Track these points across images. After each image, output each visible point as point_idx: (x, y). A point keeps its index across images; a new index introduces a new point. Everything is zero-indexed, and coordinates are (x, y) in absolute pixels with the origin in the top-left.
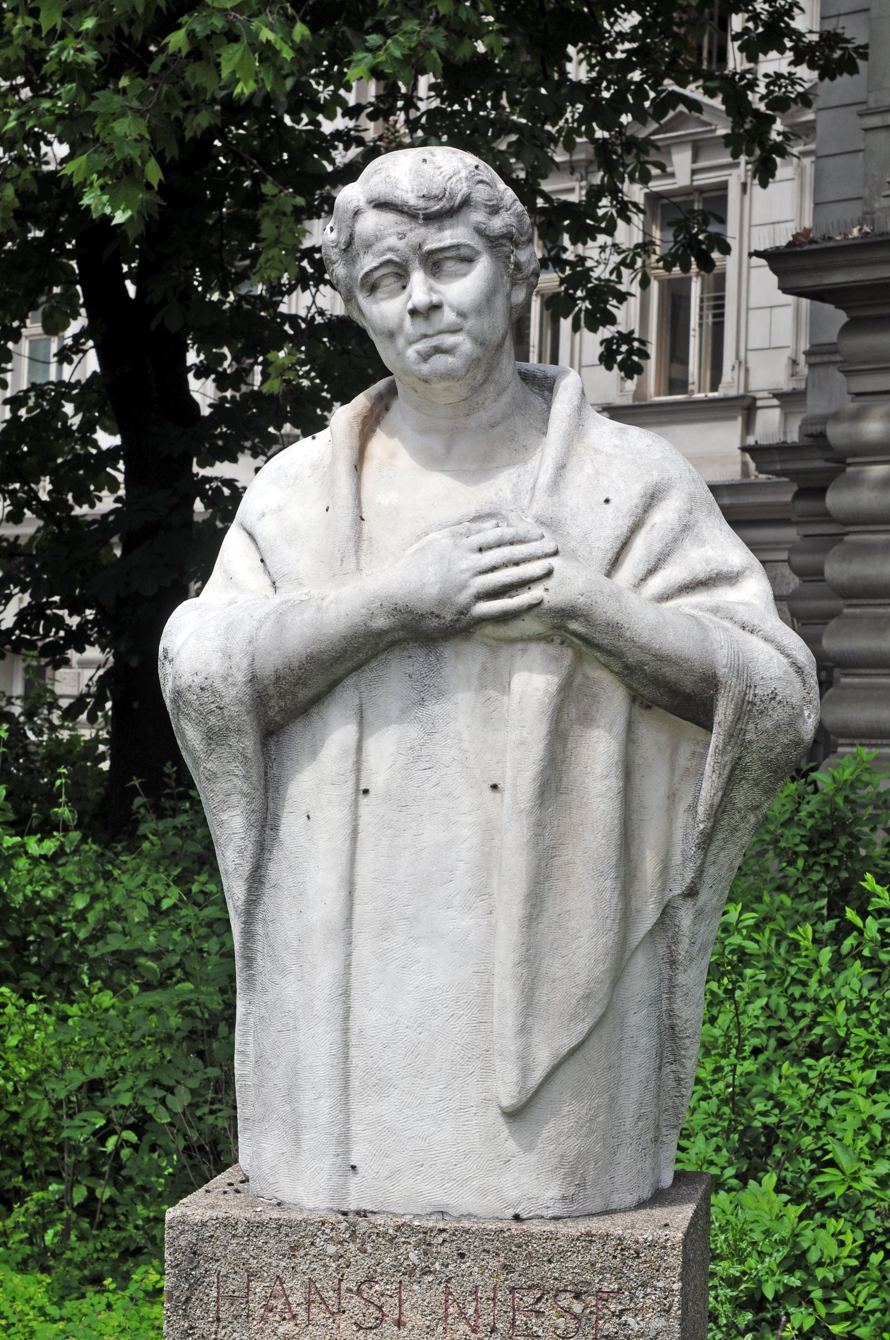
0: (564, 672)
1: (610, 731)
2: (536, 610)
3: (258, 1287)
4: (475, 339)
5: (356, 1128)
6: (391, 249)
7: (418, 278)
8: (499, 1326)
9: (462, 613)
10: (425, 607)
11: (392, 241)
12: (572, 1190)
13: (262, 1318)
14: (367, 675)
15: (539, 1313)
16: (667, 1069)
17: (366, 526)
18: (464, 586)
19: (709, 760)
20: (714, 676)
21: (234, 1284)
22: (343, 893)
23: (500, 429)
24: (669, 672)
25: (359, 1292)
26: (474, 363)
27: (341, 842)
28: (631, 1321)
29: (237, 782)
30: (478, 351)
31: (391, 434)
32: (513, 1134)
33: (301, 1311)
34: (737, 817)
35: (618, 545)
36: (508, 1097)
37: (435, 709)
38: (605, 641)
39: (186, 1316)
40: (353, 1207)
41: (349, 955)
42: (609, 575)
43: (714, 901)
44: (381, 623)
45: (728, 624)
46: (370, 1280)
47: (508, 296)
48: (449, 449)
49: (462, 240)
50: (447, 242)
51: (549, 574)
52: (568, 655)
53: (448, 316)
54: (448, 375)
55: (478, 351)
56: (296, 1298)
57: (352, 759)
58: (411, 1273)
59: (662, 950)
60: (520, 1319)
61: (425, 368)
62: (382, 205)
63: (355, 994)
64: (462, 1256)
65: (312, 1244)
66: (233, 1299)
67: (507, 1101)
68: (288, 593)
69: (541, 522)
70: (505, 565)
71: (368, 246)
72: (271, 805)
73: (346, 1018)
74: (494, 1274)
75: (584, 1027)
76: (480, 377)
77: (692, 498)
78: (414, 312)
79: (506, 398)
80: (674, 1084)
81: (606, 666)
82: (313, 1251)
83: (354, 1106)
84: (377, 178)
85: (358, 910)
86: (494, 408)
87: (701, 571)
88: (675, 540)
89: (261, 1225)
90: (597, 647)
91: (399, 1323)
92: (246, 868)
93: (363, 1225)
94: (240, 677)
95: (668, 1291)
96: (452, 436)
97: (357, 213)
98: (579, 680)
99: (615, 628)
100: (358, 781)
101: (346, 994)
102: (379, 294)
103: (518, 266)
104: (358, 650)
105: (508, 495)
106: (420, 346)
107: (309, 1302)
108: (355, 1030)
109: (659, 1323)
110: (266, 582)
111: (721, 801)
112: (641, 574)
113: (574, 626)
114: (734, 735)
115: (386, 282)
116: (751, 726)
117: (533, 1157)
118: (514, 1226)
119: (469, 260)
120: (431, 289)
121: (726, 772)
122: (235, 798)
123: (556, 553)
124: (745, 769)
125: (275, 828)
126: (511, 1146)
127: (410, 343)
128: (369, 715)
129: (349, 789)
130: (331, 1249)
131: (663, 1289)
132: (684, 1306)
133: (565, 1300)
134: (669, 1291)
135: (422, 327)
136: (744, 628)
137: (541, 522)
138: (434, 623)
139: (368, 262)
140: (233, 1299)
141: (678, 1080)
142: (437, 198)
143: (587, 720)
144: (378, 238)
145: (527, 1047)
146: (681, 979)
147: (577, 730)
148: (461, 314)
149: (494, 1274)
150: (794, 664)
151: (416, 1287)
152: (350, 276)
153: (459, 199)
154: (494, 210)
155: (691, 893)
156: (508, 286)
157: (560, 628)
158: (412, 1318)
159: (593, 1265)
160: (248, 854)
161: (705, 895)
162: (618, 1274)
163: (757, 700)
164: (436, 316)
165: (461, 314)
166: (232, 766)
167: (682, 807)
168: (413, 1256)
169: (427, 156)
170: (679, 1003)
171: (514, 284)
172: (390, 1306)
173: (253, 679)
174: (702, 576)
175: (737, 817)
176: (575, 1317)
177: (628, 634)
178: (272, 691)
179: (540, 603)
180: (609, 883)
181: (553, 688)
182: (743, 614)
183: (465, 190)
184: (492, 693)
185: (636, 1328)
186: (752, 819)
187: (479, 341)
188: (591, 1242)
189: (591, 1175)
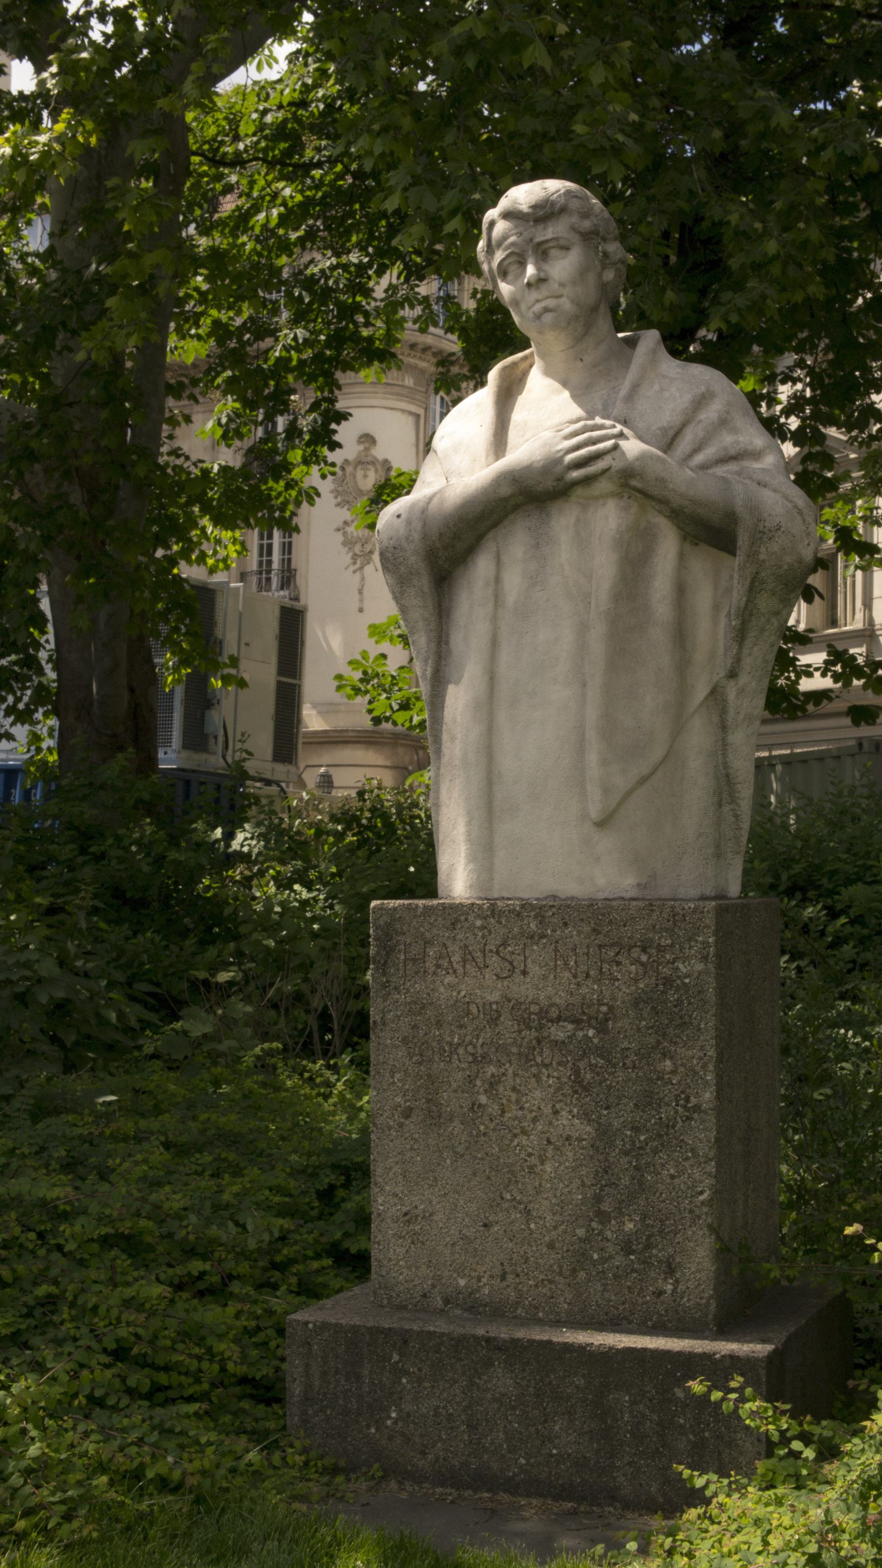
2: (608, 474)
4: (572, 302)
8: (592, 973)
9: (559, 480)
13: (434, 973)
15: (618, 963)
16: (726, 809)
21: (415, 951)
25: (498, 953)
28: (681, 966)
34: (763, 619)
36: (595, 812)
38: (655, 491)
40: (496, 895)
43: (754, 684)
45: (748, 482)
46: (504, 944)
47: (600, 275)
49: (560, 235)
56: (456, 958)
60: (606, 967)
65: (466, 920)
66: (414, 960)
72: (444, 627)
80: (734, 819)
81: (660, 512)
82: (466, 925)
91: (524, 973)
94: (416, 536)
107: (465, 961)
109: (700, 967)
111: (746, 605)
113: (634, 483)
114: (752, 555)
121: (747, 583)
125: (447, 643)
130: (479, 923)
132: (718, 955)
133: (636, 953)
134: (706, 944)
136: (759, 484)
141: (736, 816)
148: (562, 285)
151: (535, 947)
155: (732, 674)
157: (625, 485)
159: (654, 927)
163: (766, 530)
168: (533, 926)
171: (604, 267)
172: (518, 960)
173: (425, 537)
174: (732, 452)
175: (763, 619)
176: (643, 964)
177: (671, 486)
179: (608, 469)
185: (684, 970)
188: (652, 910)
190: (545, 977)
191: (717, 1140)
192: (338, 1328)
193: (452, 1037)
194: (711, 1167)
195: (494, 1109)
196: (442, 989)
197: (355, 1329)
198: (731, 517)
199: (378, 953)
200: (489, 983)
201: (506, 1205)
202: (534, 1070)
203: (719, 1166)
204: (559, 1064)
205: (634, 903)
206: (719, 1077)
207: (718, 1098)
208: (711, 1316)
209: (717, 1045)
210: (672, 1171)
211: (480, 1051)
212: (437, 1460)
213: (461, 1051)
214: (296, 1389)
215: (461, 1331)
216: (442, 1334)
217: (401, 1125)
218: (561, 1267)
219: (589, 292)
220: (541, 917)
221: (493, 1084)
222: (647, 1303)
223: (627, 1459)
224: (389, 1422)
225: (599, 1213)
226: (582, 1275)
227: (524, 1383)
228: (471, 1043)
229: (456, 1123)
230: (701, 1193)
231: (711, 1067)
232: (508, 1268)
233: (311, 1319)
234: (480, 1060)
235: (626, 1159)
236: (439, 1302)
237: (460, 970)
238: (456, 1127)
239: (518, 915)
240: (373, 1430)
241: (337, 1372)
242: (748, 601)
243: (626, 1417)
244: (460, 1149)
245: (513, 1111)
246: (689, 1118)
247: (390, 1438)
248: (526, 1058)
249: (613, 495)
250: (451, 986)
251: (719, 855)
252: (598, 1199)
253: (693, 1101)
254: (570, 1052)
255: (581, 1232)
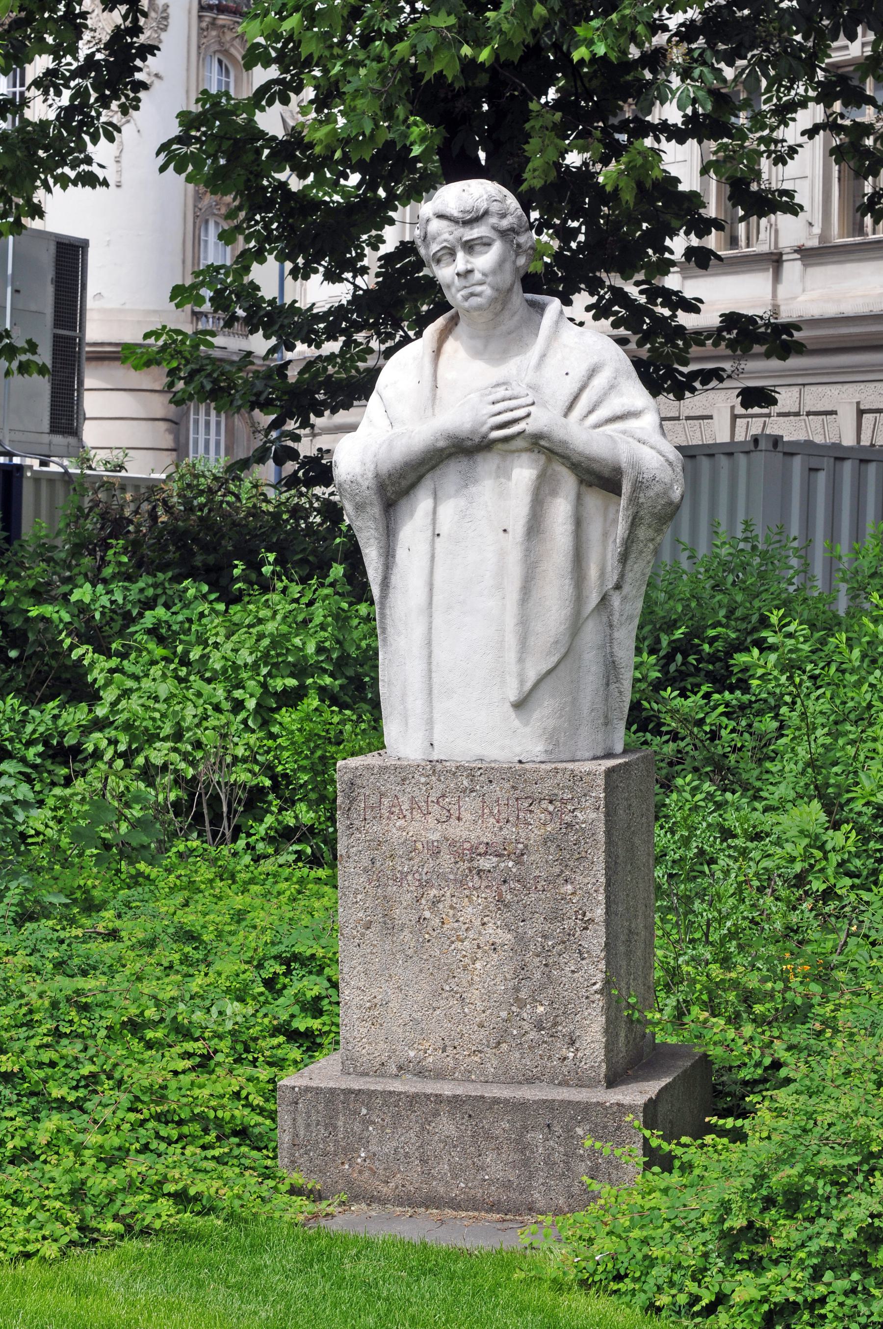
0: (540, 468)
1: (566, 499)
3: (386, 801)
4: (493, 288)
5: (436, 715)
6: (445, 241)
7: (460, 255)
10: (464, 435)
11: (446, 236)
12: (551, 747)
13: (388, 818)
14: (438, 472)
16: (613, 687)
17: (438, 391)
18: (484, 423)
19: (621, 514)
20: (620, 468)
22: (427, 589)
23: (514, 335)
24: (595, 466)
25: (438, 803)
26: (493, 301)
27: (425, 562)
28: (579, 815)
29: (372, 532)
30: (496, 294)
31: (456, 339)
32: (517, 716)
33: (407, 813)
34: (641, 545)
35: (572, 398)
36: (513, 695)
37: (473, 489)
39: (348, 818)
40: (436, 758)
41: (431, 623)
42: (566, 415)
44: (441, 444)
45: (630, 440)
46: (443, 796)
47: (514, 262)
48: (486, 346)
49: (483, 234)
50: (475, 236)
51: (528, 415)
52: (543, 459)
53: (477, 276)
54: (479, 308)
55: (496, 294)
56: (405, 807)
57: (431, 517)
58: (464, 791)
59: (605, 619)
60: (522, 814)
61: (466, 304)
62: (441, 216)
63: (434, 644)
64: (491, 782)
66: (372, 808)
67: (513, 698)
68: (398, 429)
69: (530, 387)
70: (506, 411)
71: (434, 239)
73: (430, 657)
74: (507, 791)
75: (555, 659)
76: (499, 307)
77: (617, 370)
78: (458, 274)
79: (516, 318)
82: (413, 781)
83: (435, 704)
84: (438, 201)
85: (435, 598)
86: (509, 323)
87: (618, 411)
88: (605, 394)
89: (386, 768)
90: (556, 454)
91: (459, 819)
92: (379, 579)
93: (439, 767)
94: (370, 475)
95: (598, 799)
96: (487, 339)
97: (428, 221)
98: (549, 472)
99: (564, 443)
100: (434, 529)
101: (429, 643)
102: (442, 264)
103: (519, 246)
104: (431, 459)
105: (514, 372)
106: (463, 293)
107: (412, 809)
108: (434, 663)
109: (593, 815)
110: (388, 422)
112: (584, 413)
113: (542, 443)
114: (633, 500)
115: (444, 258)
116: (642, 495)
117: (528, 729)
118: (518, 766)
119: (489, 245)
120: (467, 262)
122: (372, 541)
123: (533, 404)
124: (641, 519)
125: (394, 556)
126: (517, 723)
127: (459, 291)
128: (439, 494)
129: (429, 533)
130: (423, 780)
131: (595, 797)
132: (606, 806)
133: (544, 805)
135: (463, 282)
137: (530, 387)
138: (469, 443)
139: (435, 248)
140: (372, 808)
141: (620, 692)
142: (469, 212)
143: (554, 493)
144: (439, 235)
145: (523, 669)
146: (616, 635)
147: (549, 499)
148: (484, 274)
149: (507, 791)
150: (667, 460)
152: (427, 254)
153: (481, 211)
154: (503, 216)
155: (618, 587)
156: (514, 257)
157: (536, 444)
158: (466, 816)
160: (380, 571)
161: (626, 588)
162: (572, 790)
164: (470, 276)
165: (484, 274)
166: (369, 524)
167: (611, 540)
169: (466, 188)
170: (616, 649)
173: (377, 476)
174: (619, 413)
178: (387, 482)
179: (524, 431)
180: (567, 581)
181: (534, 477)
182: (639, 434)
183: (485, 206)
184: (503, 480)
186: (651, 546)
187: (497, 289)
189: (562, 740)
190: (475, 822)
191: (606, 944)
192: (318, 1091)
193: (403, 867)
194: (602, 966)
195: (436, 922)
196: (394, 830)
197: (332, 1091)
198: (618, 471)
199: (343, 803)
200: (432, 826)
201: (445, 995)
202: (467, 892)
203: (608, 965)
204: (486, 887)
205: (543, 766)
206: (608, 898)
207: (607, 913)
208: (602, 1076)
209: (606, 874)
210: (573, 968)
211: (425, 877)
212: (397, 1187)
213: (410, 877)
214: (285, 1138)
215: (413, 1090)
216: (400, 1093)
217: (363, 935)
218: (488, 1041)
219: (507, 277)
220: (471, 777)
221: (435, 902)
222: (554, 1067)
223: (541, 1181)
224: (359, 1160)
225: (517, 999)
226: (504, 1046)
227: (463, 1127)
228: (417, 871)
229: (406, 932)
230: (595, 984)
231: (602, 890)
232: (448, 1043)
233: (297, 1084)
234: (424, 885)
235: (538, 959)
236: (394, 1070)
237: (409, 816)
238: (406, 935)
239: (454, 774)
240: (347, 1167)
241: (318, 1125)
242: (630, 533)
243: (540, 1150)
244: (410, 952)
245: (450, 924)
246: (586, 928)
247: (360, 1172)
248: (461, 883)
249: (526, 450)
250: (401, 829)
251: (607, 723)
252: (517, 990)
253: (589, 915)
254: (494, 879)
255: (504, 1014)
